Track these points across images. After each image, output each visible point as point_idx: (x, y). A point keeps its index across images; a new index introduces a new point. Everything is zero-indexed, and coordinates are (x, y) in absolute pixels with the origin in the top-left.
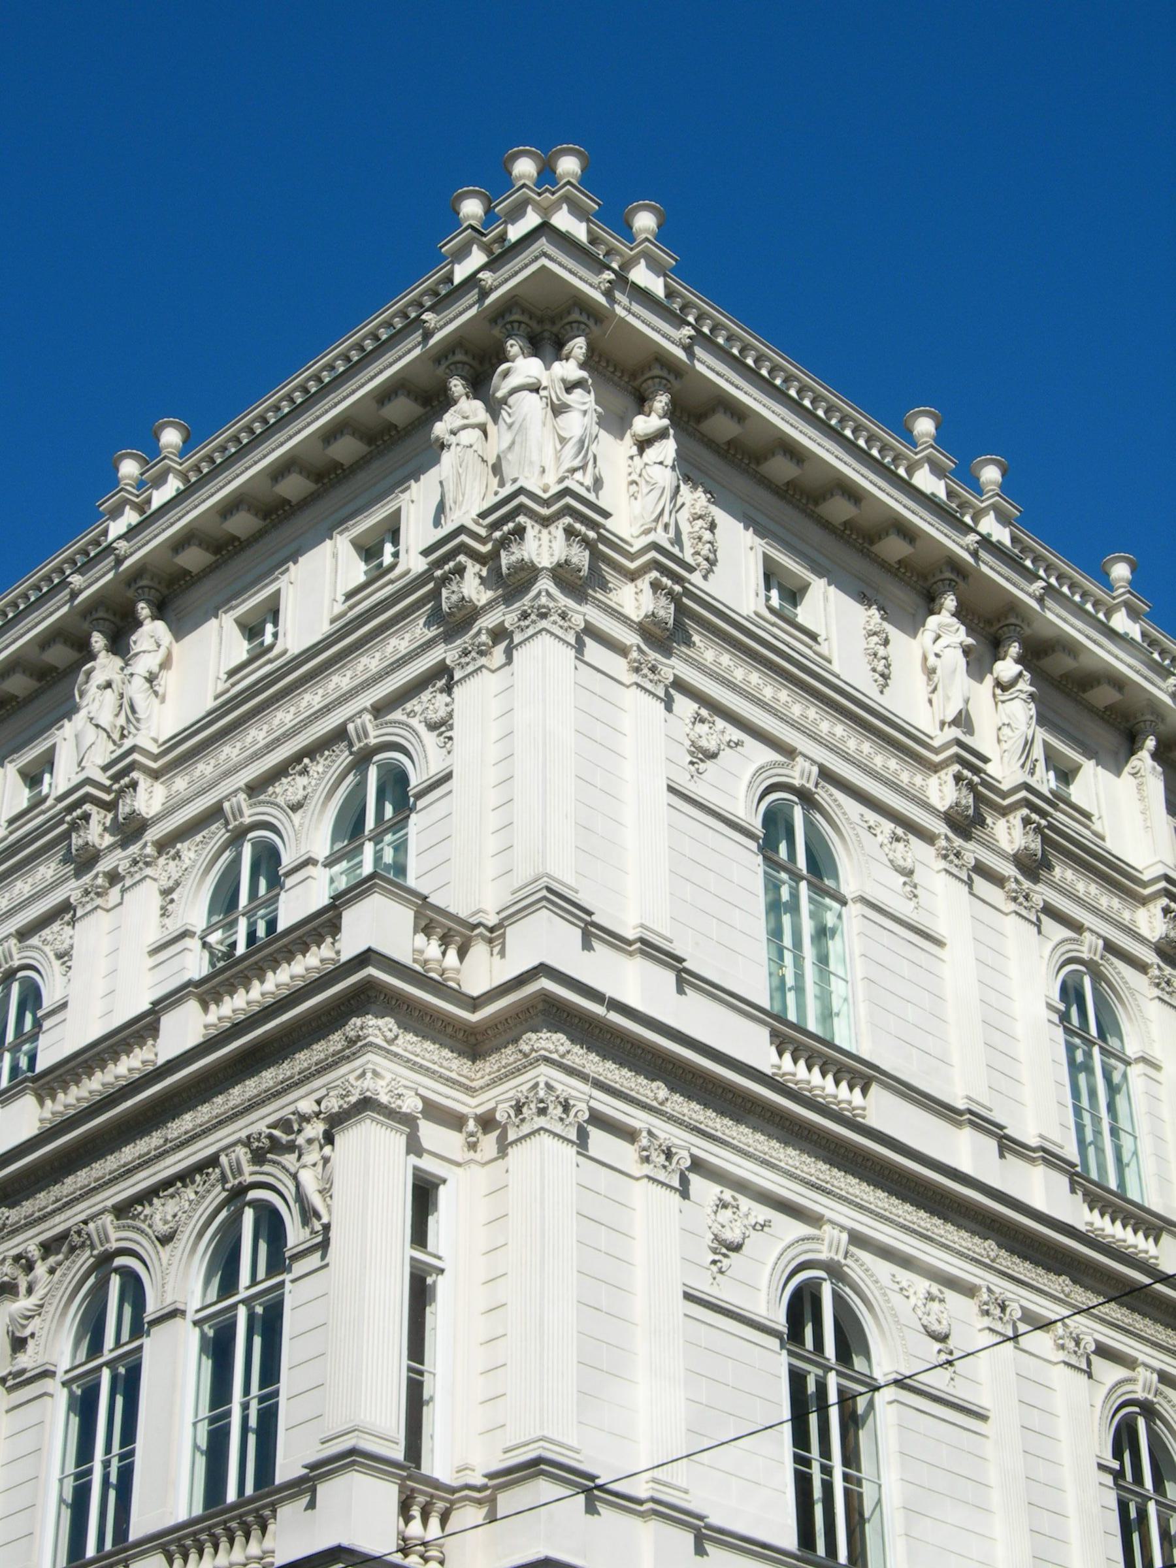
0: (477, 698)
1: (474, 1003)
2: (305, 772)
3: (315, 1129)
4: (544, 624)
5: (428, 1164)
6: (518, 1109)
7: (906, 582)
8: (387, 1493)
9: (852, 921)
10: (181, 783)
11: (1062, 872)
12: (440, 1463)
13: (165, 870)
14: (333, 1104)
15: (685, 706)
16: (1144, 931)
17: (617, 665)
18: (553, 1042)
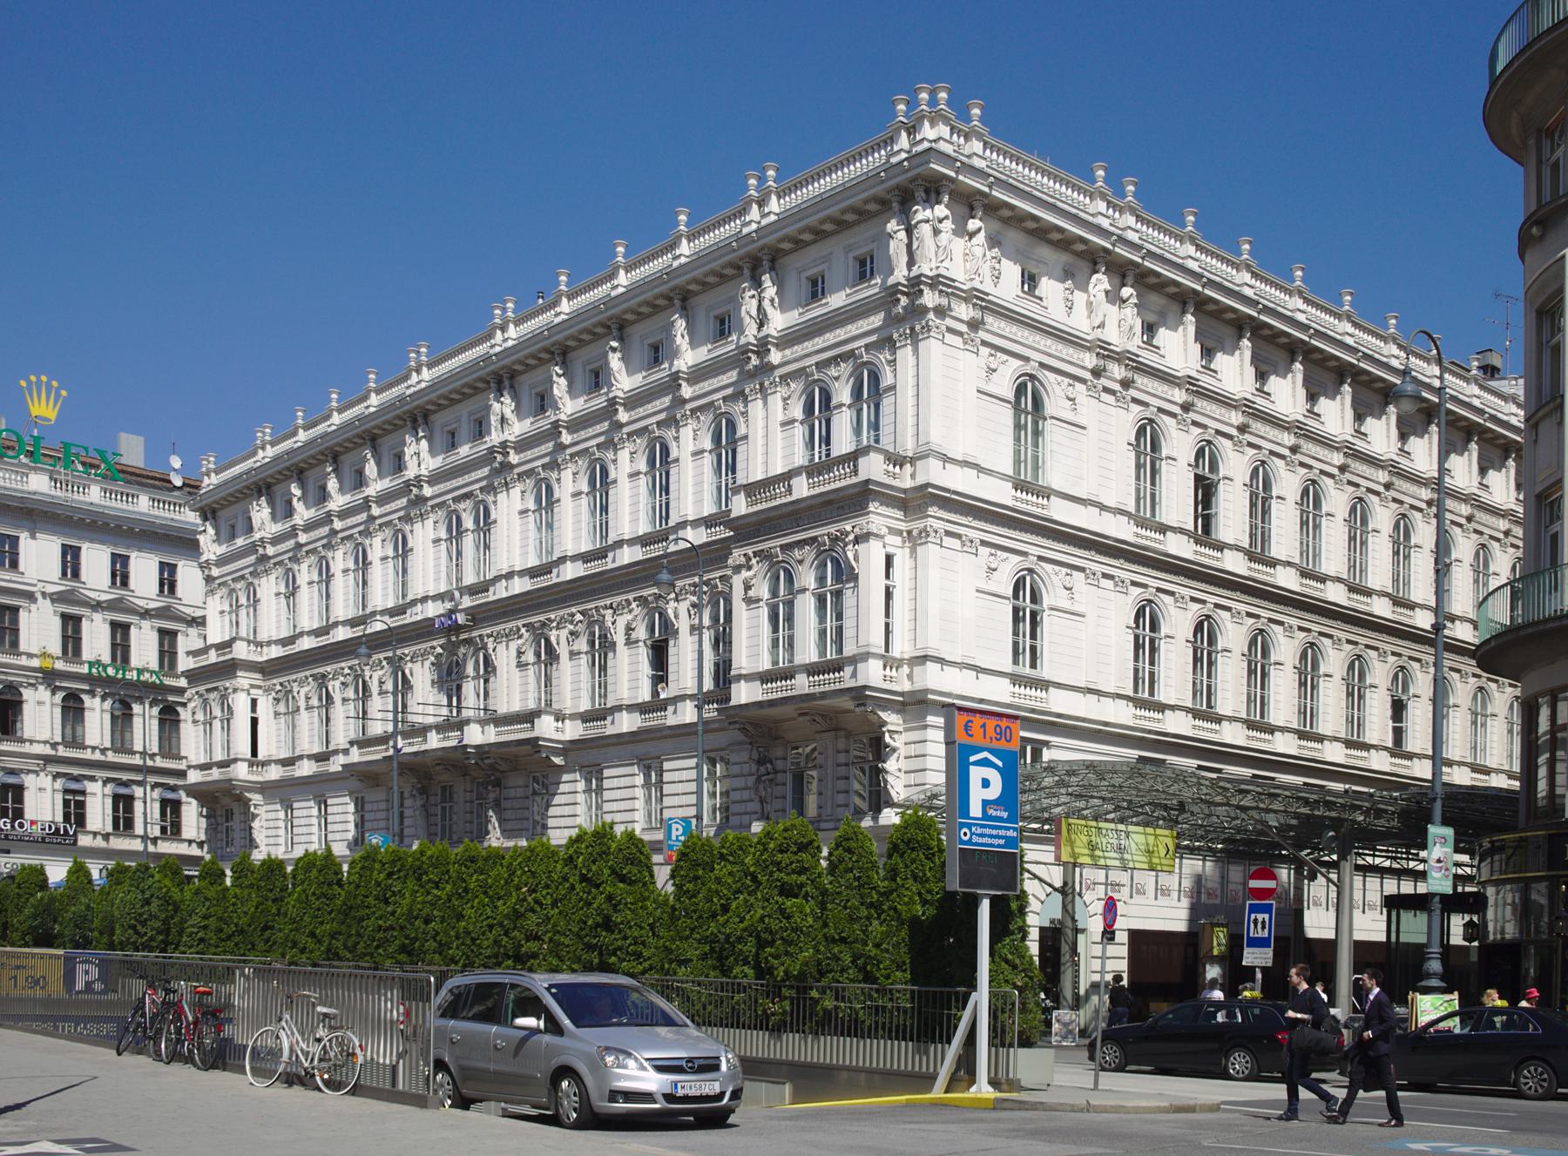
5: (890, 550)
7: (1084, 258)
8: (880, 663)
9: (1049, 426)
10: (788, 352)
12: (896, 652)
13: (782, 391)
15: (985, 351)
17: (957, 341)
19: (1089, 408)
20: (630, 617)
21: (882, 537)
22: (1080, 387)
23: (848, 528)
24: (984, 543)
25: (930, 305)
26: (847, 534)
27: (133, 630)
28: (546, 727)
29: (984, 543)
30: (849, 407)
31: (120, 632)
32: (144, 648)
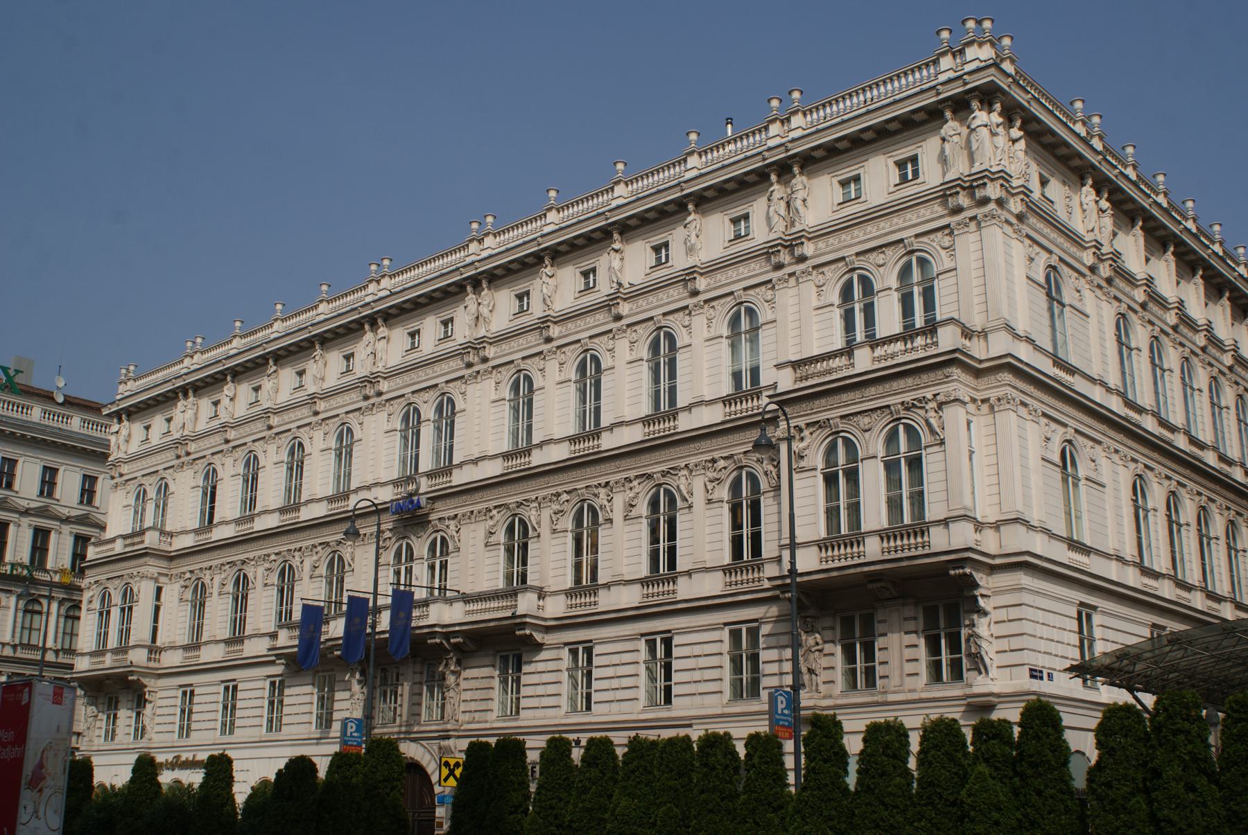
0: (968, 242)
1: (981, 362)
2: (883, 252)
3: (933, 405)
4: (994, 221)
6: (999, 400)
10: (821, 245)
11: (1032, 220)
13: (816, 277)
14: (940, 398)
15: (1028, 242)
16: (1013, 209)
18: (1007, 377)
19: (1090, 301)
20: (491, 523)
21: (965, 403)
22: (1082, 280)
23: (929, 396)
24: (1045, 415)
25: (993, 197)
26: (927, 401)
27: (53, 536)
28: (526, 603)
29: (1045, 415)
30: (896, 290)
31: (41, 537)
32: (60, 553)
